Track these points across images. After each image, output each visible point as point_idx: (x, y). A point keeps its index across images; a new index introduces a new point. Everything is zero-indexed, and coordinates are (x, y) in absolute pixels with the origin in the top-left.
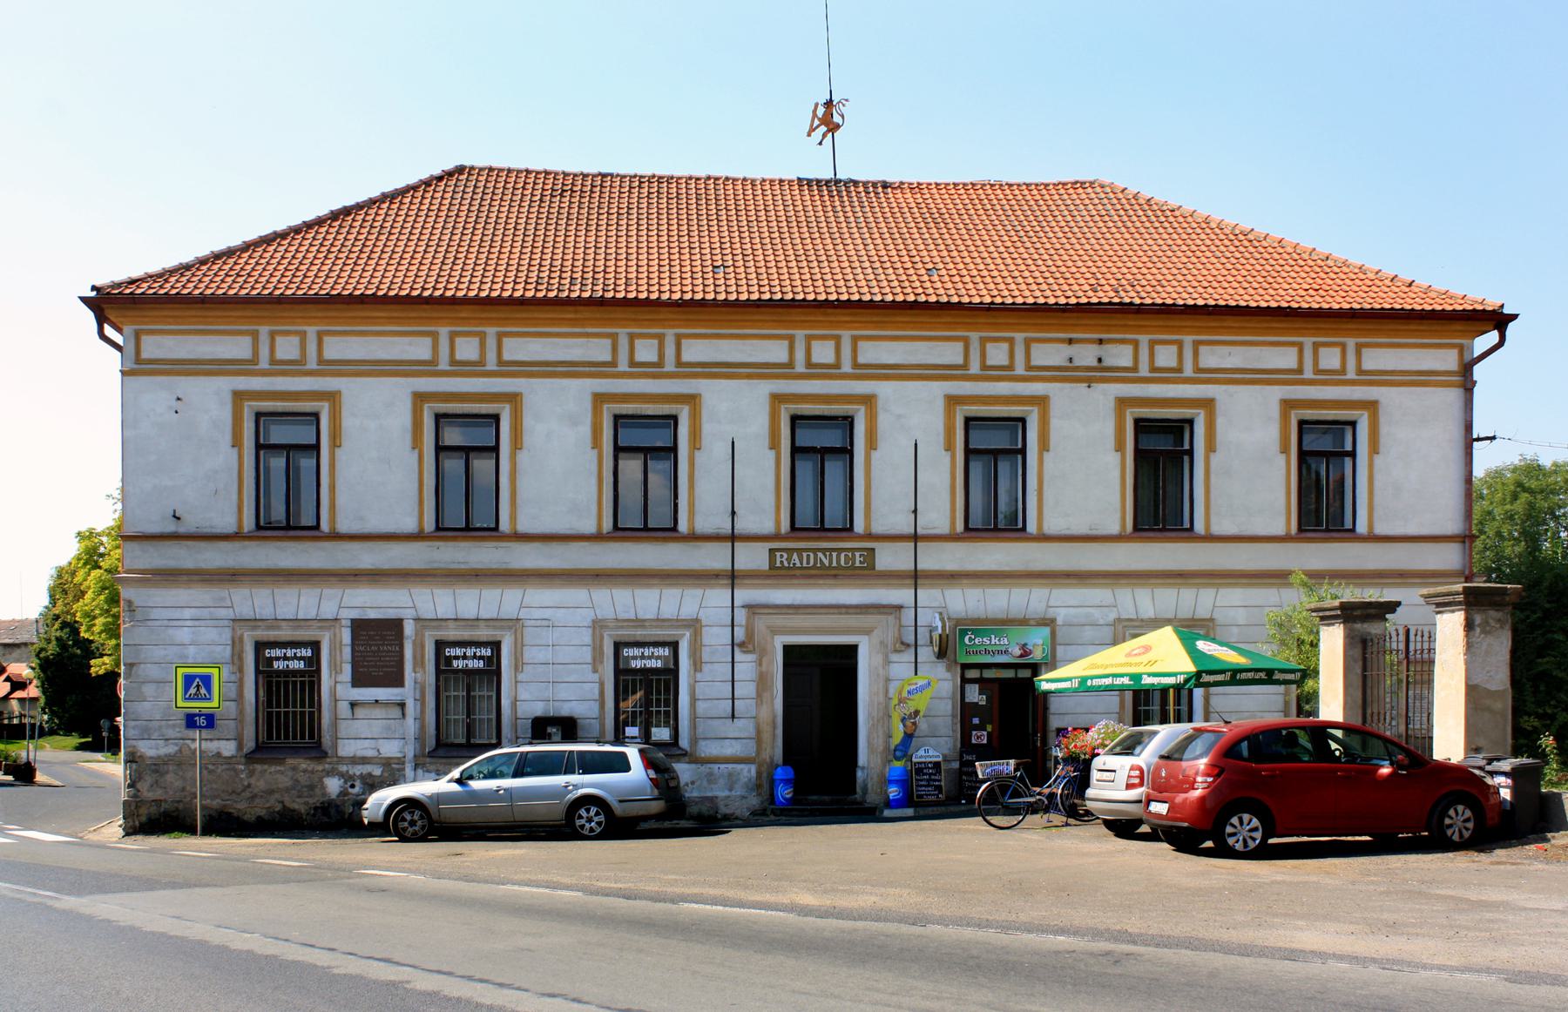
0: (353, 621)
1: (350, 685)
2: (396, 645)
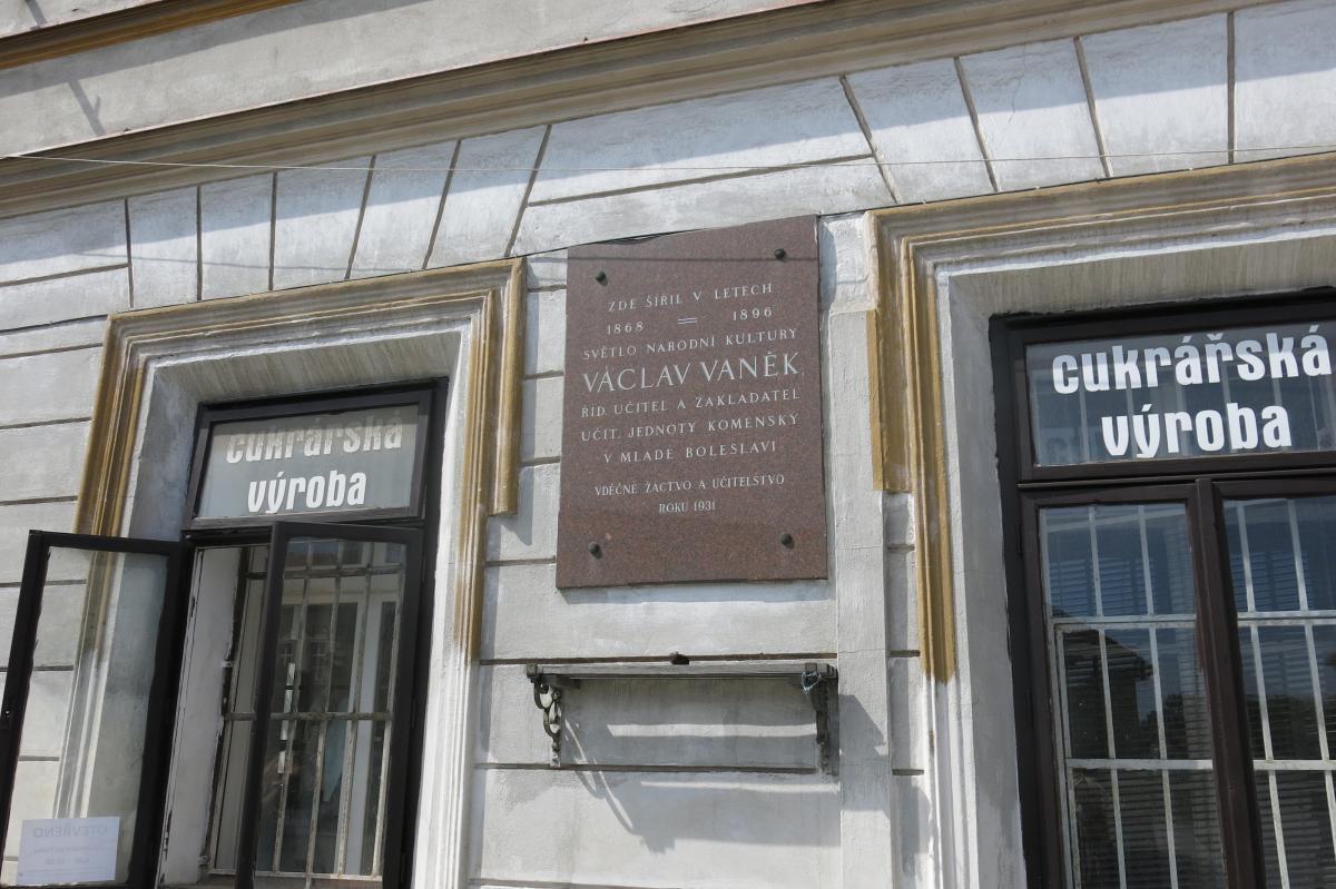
0: (577, 256)
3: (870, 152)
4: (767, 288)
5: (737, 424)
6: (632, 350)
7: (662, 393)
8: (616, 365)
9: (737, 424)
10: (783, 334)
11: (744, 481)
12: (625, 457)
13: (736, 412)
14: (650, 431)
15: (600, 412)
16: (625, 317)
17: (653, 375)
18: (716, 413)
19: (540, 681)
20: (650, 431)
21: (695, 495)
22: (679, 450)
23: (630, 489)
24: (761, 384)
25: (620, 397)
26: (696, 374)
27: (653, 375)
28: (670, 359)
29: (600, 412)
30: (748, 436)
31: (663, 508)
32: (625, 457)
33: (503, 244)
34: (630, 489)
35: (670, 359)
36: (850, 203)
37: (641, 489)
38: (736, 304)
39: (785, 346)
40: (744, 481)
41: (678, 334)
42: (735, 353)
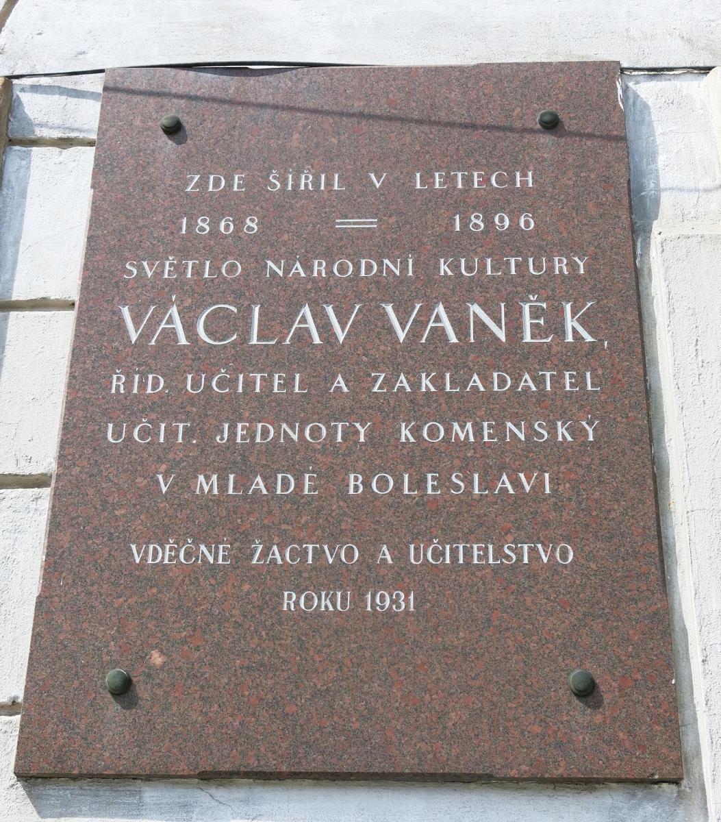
5: (463, 432)
9: (463, 432)
10: (560, 265)
11: (481, 554)
12: (206, 484)
13: (463, 407)
14: (265, 432)
18: (417, 408)
20: (265, 432)
23: (215, 555)
25: (201, 359)
26: (373, 326)
28: (319, 292)
31: (290, 601)
32: (206, 484)
34: (215, 555)
35: (319, 292)
37: (241, 556)
40: (481, 554)
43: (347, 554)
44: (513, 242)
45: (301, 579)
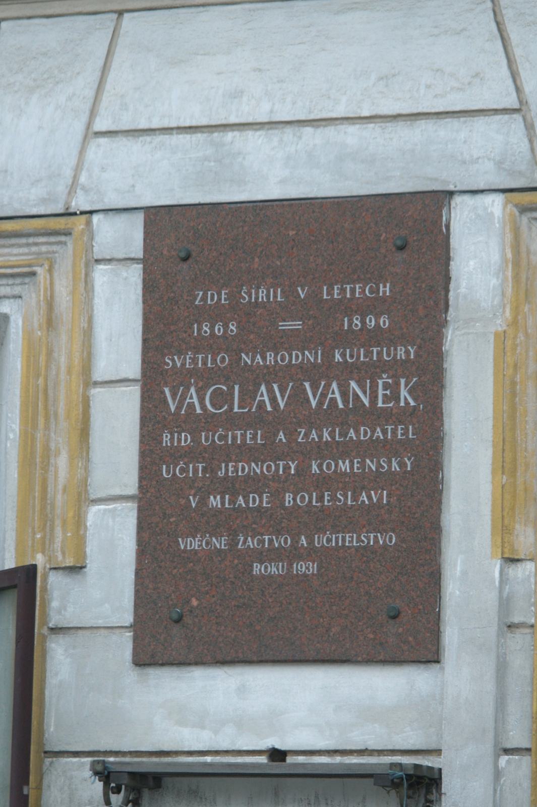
1: (125, 645)
2: (397, 369)
3: (511, 101)
4: (385, 290)
6: (223, 360)
7: (259, 419)
8: (205, 378)
10: (401, 353)
11: (350, 540)
12: (214, 501)
13: (344, 450)
14: (244, 468)
15: (185, 439)
16: (216, 314)
17: (248, 395)
19: (105, 774)
20: (244, 468)
21: (293, 555)
22: (278, 495)
23: (220, 543)
24: (374, 416)
25: (209, 422)
26: (299, 397)
27: (248, 395)
28: (270, 375)
29: (185, 439)
30: (358, 483)
31: (257, 569)
32: (214, 501)
33: (61, 189)
35: (270, 375)
36: (487, 176)
37: (233, 543)
38: (348, 307)
39: (397, 369)
40: (350, 540)
41: (282, 341)
42: (349, 371)
43: (282, 541)
44: (375, 337)
45: (262, 556)
